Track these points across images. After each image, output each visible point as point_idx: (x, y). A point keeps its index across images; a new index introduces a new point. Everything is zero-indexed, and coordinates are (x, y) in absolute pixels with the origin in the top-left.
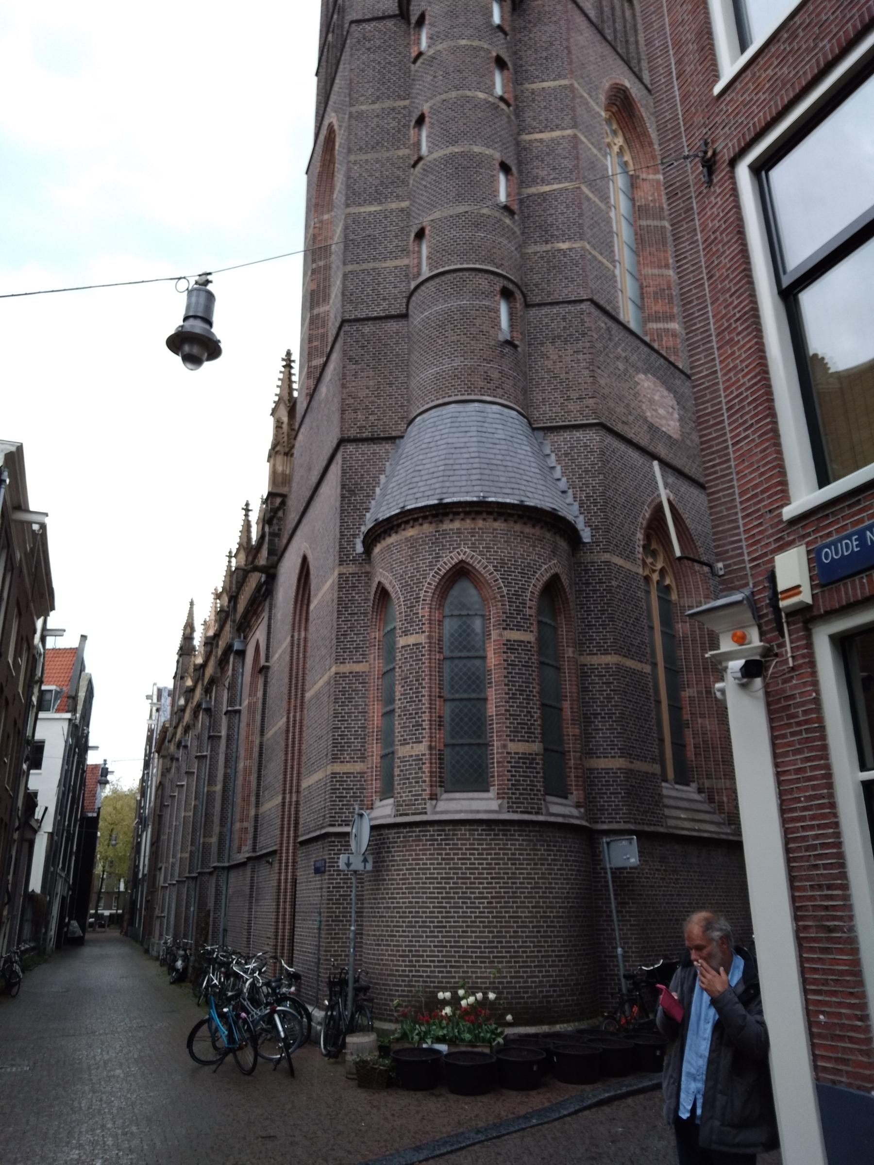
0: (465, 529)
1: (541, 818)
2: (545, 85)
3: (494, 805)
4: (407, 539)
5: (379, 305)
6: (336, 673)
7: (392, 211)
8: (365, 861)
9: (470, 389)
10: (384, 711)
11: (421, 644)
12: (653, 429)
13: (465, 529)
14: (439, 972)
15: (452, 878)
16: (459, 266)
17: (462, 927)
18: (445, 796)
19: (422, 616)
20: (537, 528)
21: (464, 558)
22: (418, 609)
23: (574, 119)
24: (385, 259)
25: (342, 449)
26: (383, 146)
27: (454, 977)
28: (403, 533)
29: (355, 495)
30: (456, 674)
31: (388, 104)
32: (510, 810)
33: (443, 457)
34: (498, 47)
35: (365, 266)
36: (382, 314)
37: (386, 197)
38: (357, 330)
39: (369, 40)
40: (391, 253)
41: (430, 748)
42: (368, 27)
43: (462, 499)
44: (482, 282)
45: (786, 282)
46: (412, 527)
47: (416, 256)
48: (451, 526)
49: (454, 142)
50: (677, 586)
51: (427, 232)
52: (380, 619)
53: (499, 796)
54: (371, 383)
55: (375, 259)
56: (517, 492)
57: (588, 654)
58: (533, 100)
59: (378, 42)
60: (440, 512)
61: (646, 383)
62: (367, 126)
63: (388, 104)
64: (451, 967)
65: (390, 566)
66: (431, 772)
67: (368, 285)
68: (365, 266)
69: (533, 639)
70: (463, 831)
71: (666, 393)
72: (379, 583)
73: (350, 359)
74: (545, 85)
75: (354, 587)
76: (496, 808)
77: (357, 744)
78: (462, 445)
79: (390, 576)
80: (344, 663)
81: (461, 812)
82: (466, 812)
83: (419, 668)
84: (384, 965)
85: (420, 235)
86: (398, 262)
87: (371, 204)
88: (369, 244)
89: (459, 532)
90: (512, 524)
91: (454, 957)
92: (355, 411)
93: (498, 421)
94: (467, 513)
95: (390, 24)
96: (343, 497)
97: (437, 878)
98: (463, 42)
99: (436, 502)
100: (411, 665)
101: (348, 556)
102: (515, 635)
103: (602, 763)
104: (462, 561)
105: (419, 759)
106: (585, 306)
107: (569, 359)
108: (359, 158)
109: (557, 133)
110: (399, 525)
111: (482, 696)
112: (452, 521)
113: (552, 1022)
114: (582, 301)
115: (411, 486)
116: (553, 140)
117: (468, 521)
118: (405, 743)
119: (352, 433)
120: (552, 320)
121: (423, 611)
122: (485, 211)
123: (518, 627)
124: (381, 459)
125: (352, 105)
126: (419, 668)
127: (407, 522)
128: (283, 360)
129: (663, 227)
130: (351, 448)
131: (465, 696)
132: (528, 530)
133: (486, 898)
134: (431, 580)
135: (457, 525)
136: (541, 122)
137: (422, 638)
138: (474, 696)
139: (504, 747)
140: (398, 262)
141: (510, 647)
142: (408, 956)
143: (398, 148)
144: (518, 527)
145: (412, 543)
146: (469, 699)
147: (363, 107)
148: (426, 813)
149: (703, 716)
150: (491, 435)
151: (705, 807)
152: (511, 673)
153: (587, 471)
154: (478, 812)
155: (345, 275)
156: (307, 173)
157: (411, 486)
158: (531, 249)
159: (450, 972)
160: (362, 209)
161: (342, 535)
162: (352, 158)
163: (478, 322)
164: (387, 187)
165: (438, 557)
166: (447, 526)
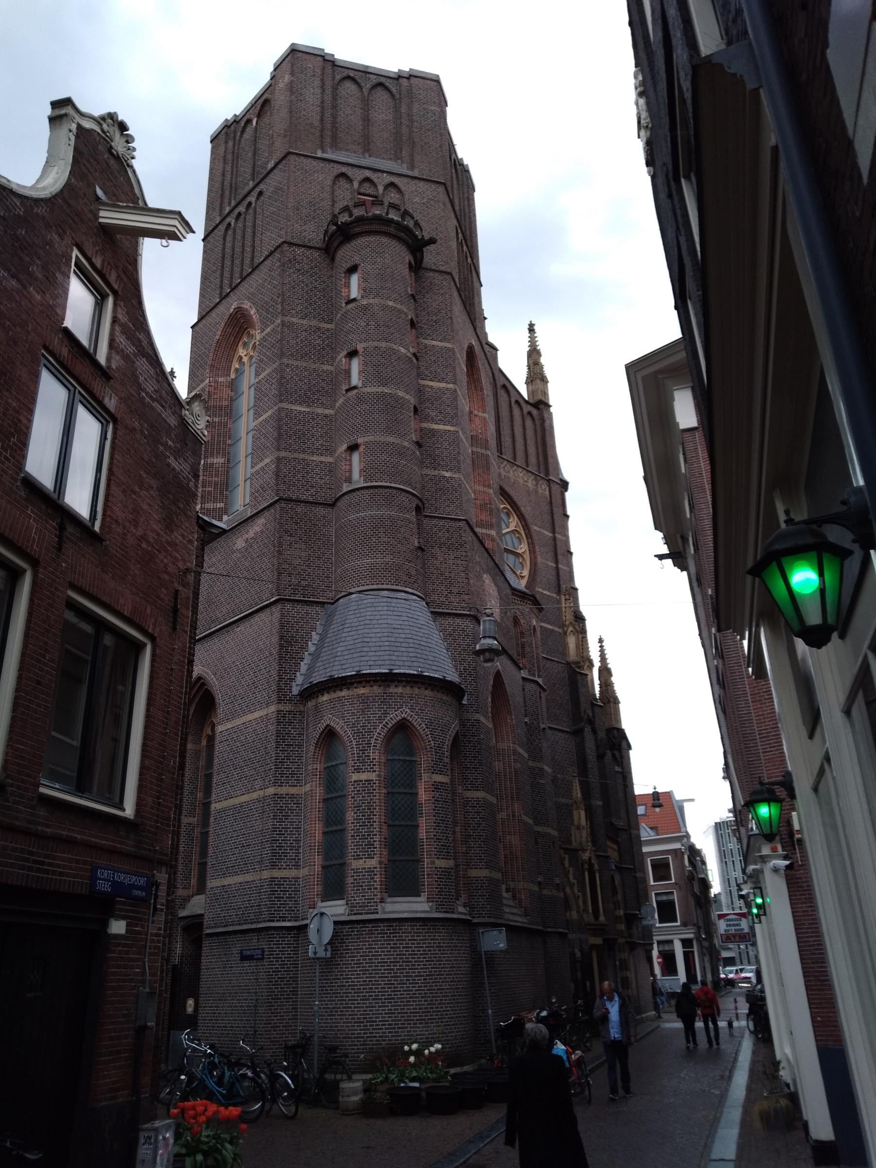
1: (455, 916)
2: (435, 343)
3: (426, 907)
4: (359, 696)
7: (318, 415)
8: (326, 950)
9: (397, 582)
10: (326, 830)
14: (389, 1033)
15: (399, 962)
16: (388, 484)
17: (406, 998)
18: (389, 900)
23: (454, 376)
24: (313, 453)
26: (310, 358)
27: (401, 1036)
28: (355, 690)
30: (396, 806)
31: (314, 323)
32: (438, 910)
33: (386, 634)
35: (296, 455)
36: (311, 500)
37: (313, 402)
39: (299, 263)
40: (318, 449)
41: (380, 863)
42: (299, 251)
43: (407, 672)
44: (404, 499)
47: (347, 463)
48: (396, 690)
49: (385, 385)
53: (429, 900)
54: (303, 554)
55: (304, 452)
58: (426, 353)
59: (306, 267)
60: (389, 679)
61: (487, 579)
62: (297, 337)
63: (314, 323)
64: (398, 1028)
65: (337, 713)
66: (381, 881)
68: (296, 455)
69: (448, 782)
70: (406, 926)
72: (328, 725)
73: (286, 532)
74: (435, 343)
76: (428, 909)
77: (292, 854)
78: (399, 627)
81: (405, 912)
82: (408, 912)
84: (338, 1030)
86: (323, 459)
87: (300, 404)
88: (300, 438)
89: (401, 696)
90: (436, 693)
91: (400, 1020)
92: (290, 575)
94: (408, 682)
96: (281, 646)
97: (387, 962)
98: (391, 303)
99: (387, 671)
102: (439, 778)
103: (474, 873)
104: (404, 718)
105: (371, 871)
106: (462, 524)
107: (451, 562)
108: (290, 362)
109: (443, 385)
110: (352, 684)
111: (414, 823)
113: (461, 1065)
114: (460, 520)
115: (363, 654)
116: (439, 389)
117: (408, 688)
118: (358, 858)
120: (440, 530)
122: (406, 444)
123: (441, 772)
124: (312, 618)
127: (360, 682)
129: (487, 456)
131: (403, 823)
132: (445, 698)
133: (423, 976)
135: (400, 690)
136: (431, 372)
138: (409, 823)
139: (431, 863)
140: (323, 459)
141: (437, 787)
142: (363, 1022)
143: (323, 363)
144: (439, 695)
145: (364, 699)
146: (406, 826)
147: (294, 320)
148: (377, 913)
149: (510, 834)
151: (511, 903)
154: (417, 912)
155: (279, 460)
159: (398, 1032)
160: (294, 407)
161: (281, 679)
162: (285, 360)
163: (402, 530)
164: (314, 394)
165: (386, 714)
166: (392, 690)
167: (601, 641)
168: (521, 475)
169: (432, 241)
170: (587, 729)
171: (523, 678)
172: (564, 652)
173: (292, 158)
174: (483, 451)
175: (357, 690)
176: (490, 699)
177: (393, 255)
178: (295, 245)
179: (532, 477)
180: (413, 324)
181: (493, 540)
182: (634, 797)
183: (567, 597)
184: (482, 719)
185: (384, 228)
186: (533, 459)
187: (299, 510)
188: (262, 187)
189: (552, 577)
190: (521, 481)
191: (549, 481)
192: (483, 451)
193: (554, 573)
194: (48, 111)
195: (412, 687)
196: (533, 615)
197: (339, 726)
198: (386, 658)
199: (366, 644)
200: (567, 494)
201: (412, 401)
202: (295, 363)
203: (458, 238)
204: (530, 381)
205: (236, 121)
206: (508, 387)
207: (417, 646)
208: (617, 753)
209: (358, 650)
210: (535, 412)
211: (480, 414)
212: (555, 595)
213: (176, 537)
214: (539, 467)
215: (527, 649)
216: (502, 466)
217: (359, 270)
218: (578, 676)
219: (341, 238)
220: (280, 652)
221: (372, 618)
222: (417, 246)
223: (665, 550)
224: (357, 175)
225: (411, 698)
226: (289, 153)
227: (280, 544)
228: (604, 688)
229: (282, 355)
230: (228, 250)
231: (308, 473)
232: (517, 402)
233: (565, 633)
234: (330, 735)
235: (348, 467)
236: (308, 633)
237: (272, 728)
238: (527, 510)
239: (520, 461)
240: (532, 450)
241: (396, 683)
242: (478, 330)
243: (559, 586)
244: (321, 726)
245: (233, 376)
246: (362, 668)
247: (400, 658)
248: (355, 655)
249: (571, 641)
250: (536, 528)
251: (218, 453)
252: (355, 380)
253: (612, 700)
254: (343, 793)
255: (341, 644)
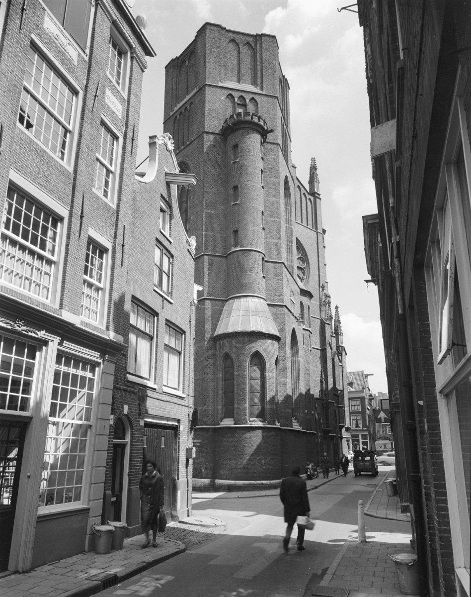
167: (337, 308)
169: (272, 131)
186: (310, 222)
188: (193, 100)
194: (148, 140)
208: (340, 357)
213: (365, 443)
223: (369, 277)
224: (236, 95)
239: (304, 223)
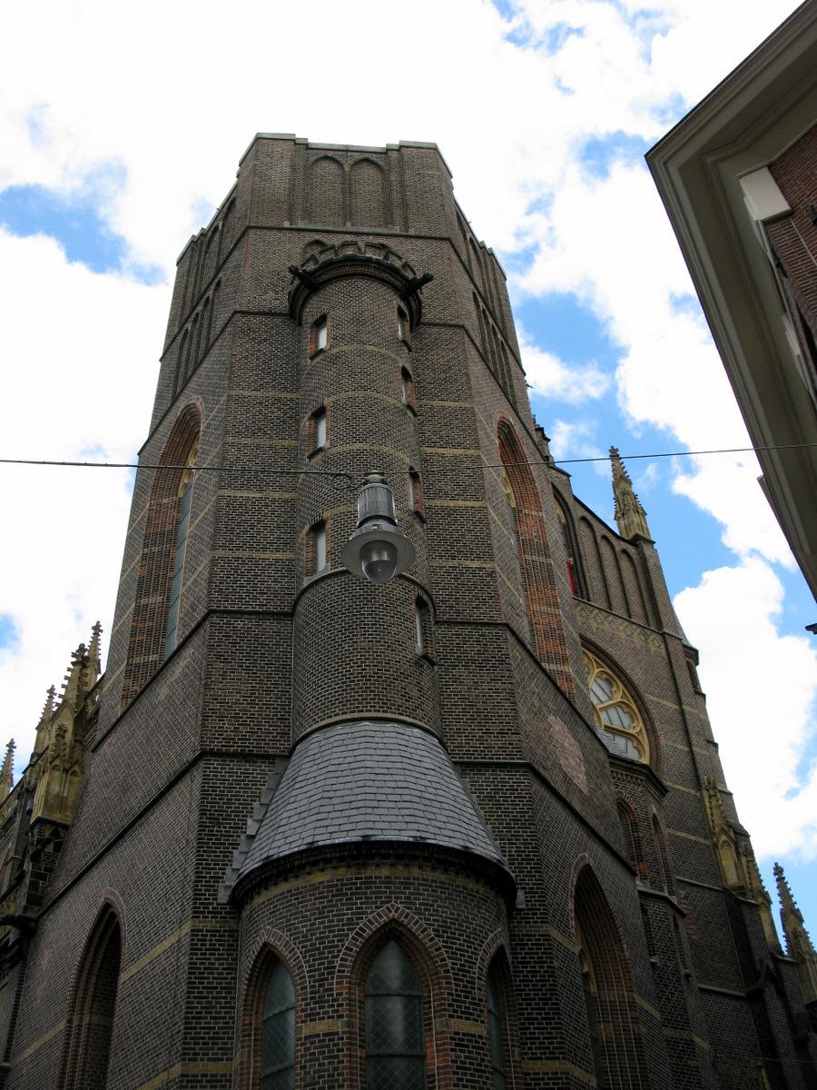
0: (396, 878)
2: (446, 404)
5: (255, 598)
6: (182, 1075)
7: (274, 501)
11: (337, 1033)
12: (567, 780)
13: (396, 878)
19: (338, 994)
20: (481, 884)
21: (396, 915)
22: (332, 984)
23: (476, 440)
24: (264, 549)
25: (202, 764)
26: (265, 433)
29: (219, 825)
34: (404, 361)
35: (239, 554)
38: (228, 623)
42: (254, 320)
45: (667, 637)
46: (322, 870)
48: (377, 873)
50: (596, 974)
51: (328, 526)
52: (260, 997)
56: (458, 835)
57: (530, 1059)
60: (365, 852)
67: (242, 575)
68: (239, 554)
69: (484, 1034)
71: (573, 741)
72: (265, 944)
75: (213, 949)
78: (385, 771)
79: (286, 936)
80: (196, 1060)
83: (335, 1069)
85: (318, 527)
90: (453, 876)
93: (423, 747)
95: (278, 320)
96: (202, 826)
100: (320, 1065)
101: (206, 906)
104: (393, 919)
107: (485, 686)
110: (302, 867)
112: (378, 865)
115: (320, 817)
116: (455, 457)
119: (215, 746)
121: (339, 987)
123: (467, 1015)
125: (230, 388)
126: (335, 1069)
127: (314, 864)
128: (74, 655)
130: (215, 763)
132: (472, 885)
134: (351, 944)
135: (385, 872)
136: (441, 437)
137: (339, 1026)
144: (460, 881)
147: (246, 393)
150: (418, 763)
152: (462, 1080)
153: (515, 820)
155: (214, 561)
156: (139, 454)
157: (320, 817)
158: (159, 599)
161: (199, 878)
162: (230, 439)
166: (371, 872)
167: (778, 871)
168: (621, 628)
169: (427, 279)
170: (770, 992)
171: (641, 893)
172: (718, 874)
173: (251, 233)
174: (542, 559)
175: (310, 878)
176: (571, 906)
177: (382, 304)
178: (250, 313)
179: (639, 630)
180: (406, 374)
181: (569, 679)
182: (661, 431)
183: (712, 792)
184: (555, 934)
185: (360, 269)
186: (636, 608)
187: (239, 624)
189: (685, 763)
190: (623, 635)
191: (663, 635)
192: (542, 559)
193: (688, 759)
195: (407, 866)
196: (651, 799)
197: (282, 942)
198: (359, 818)
199: (327, 801)
200: (699, 669)
201: (407, 460)
202: (243, 441)
203: (478, 307)
204: (621, 514)
205: (203, 234)
206: (590, 519)
207: (417, 800)
209: (313, 812)
210: (632, 550)
211: (534, 513)
212: (693, 792)
214: (647, 619)
215: (646, 849)
216: (593, 615)
217: (329, 324)
218: (744, 908)
219: (306, 291)
220: (199, 838)
221: (341, 761)
222: (409, 290)
225: (407, 884)
226: (249, 228)
227: (209, 675)
228: (793, 942)
229: (227, 433)
230: (184, 358)
231: (256, 575)
232: (604, 537)
233: (716, 846)
234: (269, 961)
235: (310, 555)
236: (247, 805)
237: (184, 960)
238: (637, 675)
240: (634, 598)
241: (377, 860)
242: (519, 407)
243: (697, 776)
244: (256, 948)
245: (181, 494)
246: (316, 838)
247: (384, 818)
248: (307, 821)
249: (728, 860)
250: (652, 698)
251: (155, 590)
252: (323, 441)
253: (807, 957)
254: (287, 1064)
255: (289, 807)
